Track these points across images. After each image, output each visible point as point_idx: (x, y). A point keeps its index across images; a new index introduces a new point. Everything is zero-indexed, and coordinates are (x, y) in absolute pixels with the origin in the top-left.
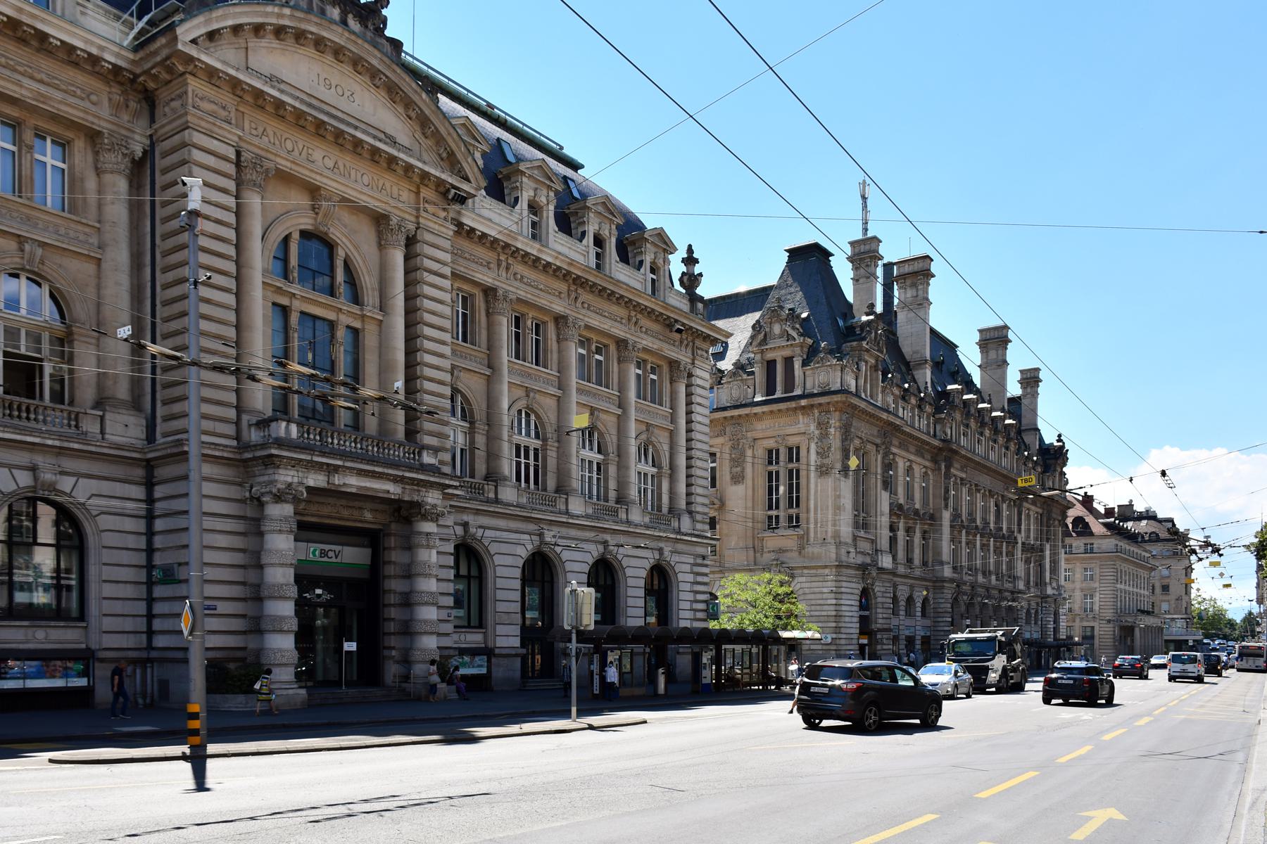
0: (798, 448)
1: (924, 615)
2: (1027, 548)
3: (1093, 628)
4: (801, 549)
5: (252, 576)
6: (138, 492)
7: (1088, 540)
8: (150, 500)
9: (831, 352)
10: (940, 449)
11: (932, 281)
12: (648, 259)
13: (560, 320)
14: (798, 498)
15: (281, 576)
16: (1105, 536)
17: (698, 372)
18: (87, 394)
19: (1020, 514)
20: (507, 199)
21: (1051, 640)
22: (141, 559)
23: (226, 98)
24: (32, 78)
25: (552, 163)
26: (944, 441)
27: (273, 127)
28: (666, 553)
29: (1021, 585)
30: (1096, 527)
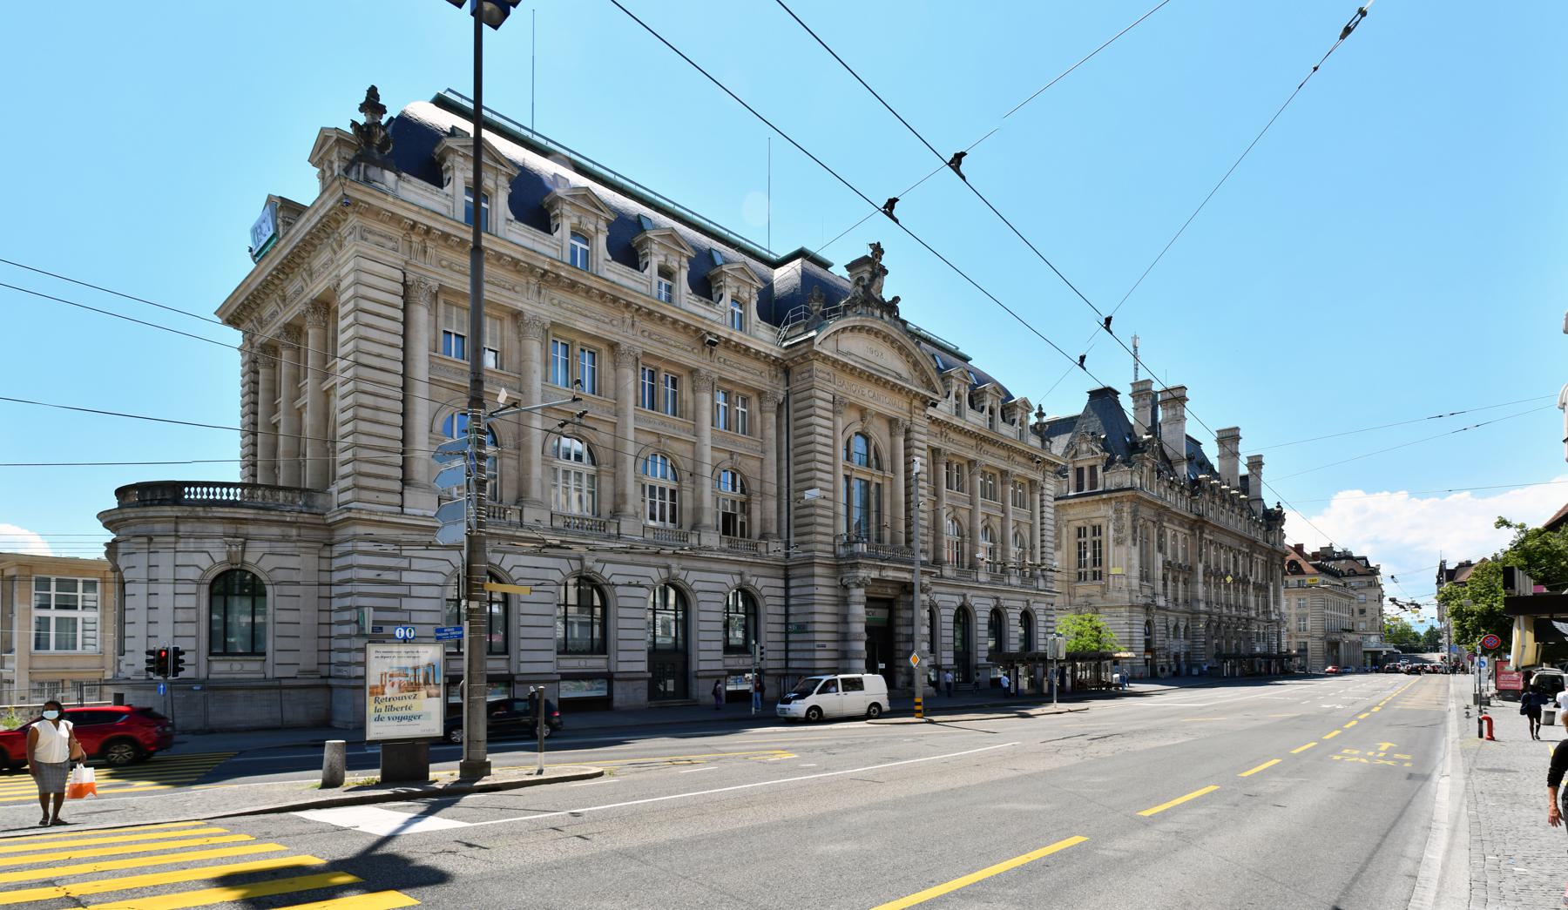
0: (1100, 526)
1: (1185, 638)
2: (1257, 587)
3: (1306, 643)
4: (1103, 594)
5: (841, 628)
6: (781, 583)
7: (1301, 578)
8: (787, 588)
9: (1124, 462)
10: (1195, 521)
11: (1241, 441)
12: (1018, 418)
13: (971, 463)
14: (1100, 560)
15: (859, 628)
16: (1315, 574)
17: (1048, 486)
18: (756, 531)
19: (1251, 562)
20: (714, 296)
21: (1276, 653)
22: (782, 619)
23: (829, 368)
24: (739, 369)
25: (753, 263)
26: (1198, 515)
27: (848, 379)
28: (968, 597)
29: (1253, 614)
30: (1307, 567)
